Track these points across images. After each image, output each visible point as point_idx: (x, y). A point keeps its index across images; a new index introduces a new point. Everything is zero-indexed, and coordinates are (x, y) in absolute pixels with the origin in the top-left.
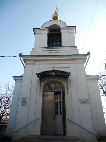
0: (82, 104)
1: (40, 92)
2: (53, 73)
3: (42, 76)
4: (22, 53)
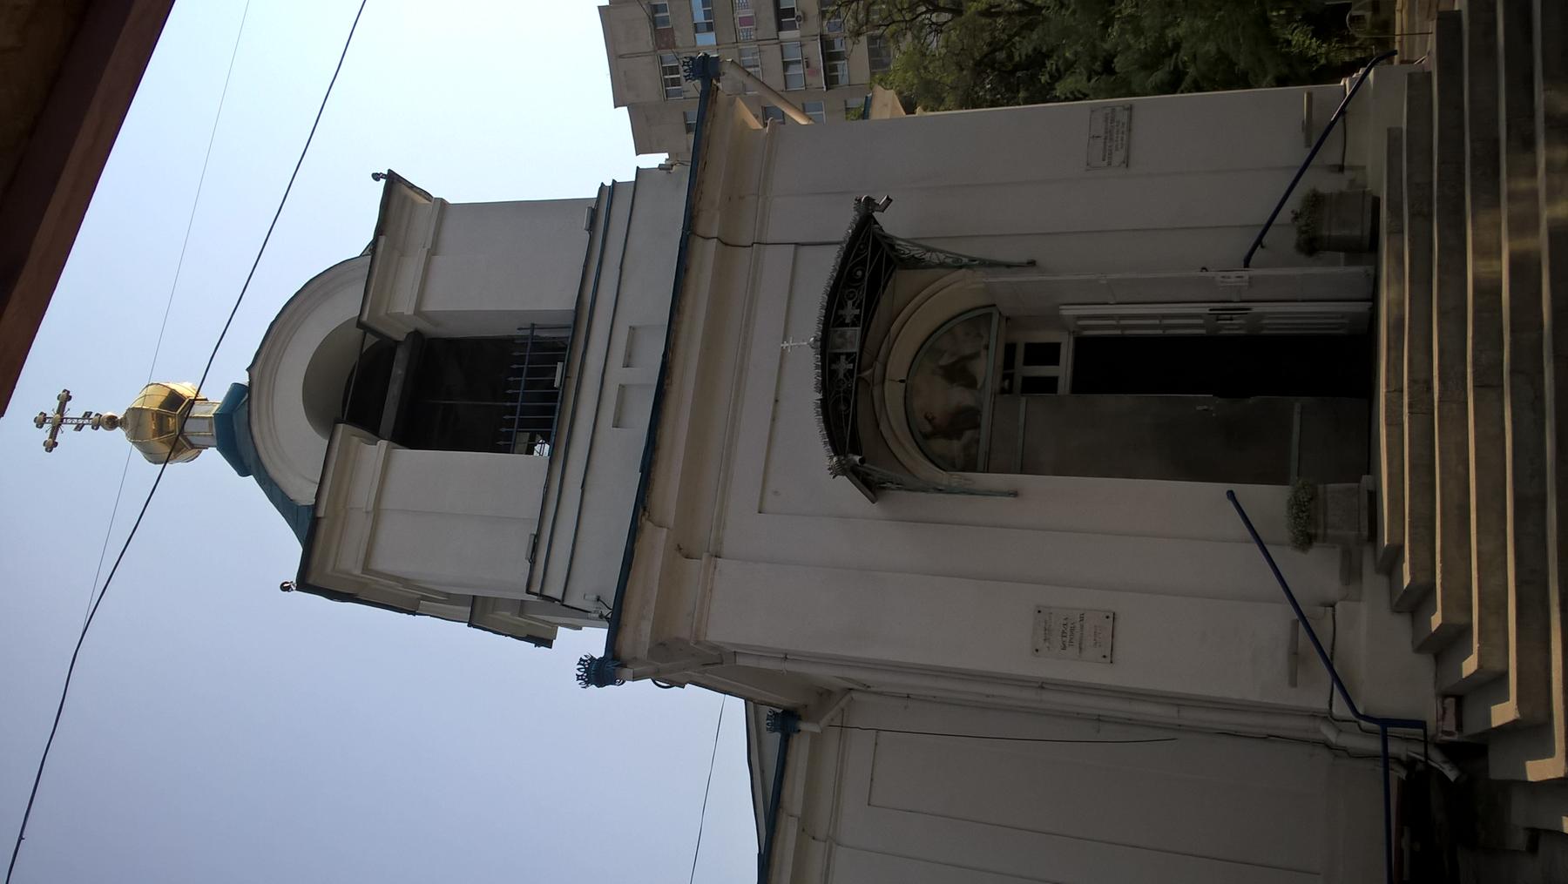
0: (1128, 150)
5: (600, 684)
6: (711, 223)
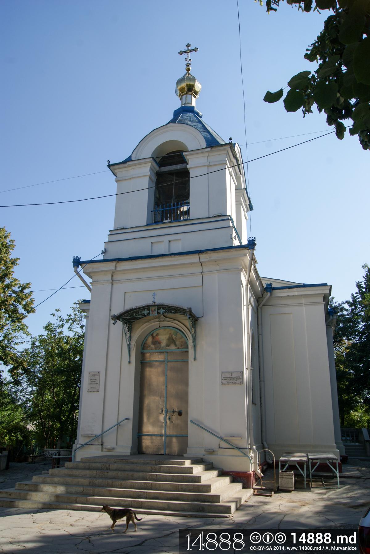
1: (130, 356)
2: (152, 311)
3: (129, 318)
4: (79, 256)
5: (73, 262)
6: (204, 257)
